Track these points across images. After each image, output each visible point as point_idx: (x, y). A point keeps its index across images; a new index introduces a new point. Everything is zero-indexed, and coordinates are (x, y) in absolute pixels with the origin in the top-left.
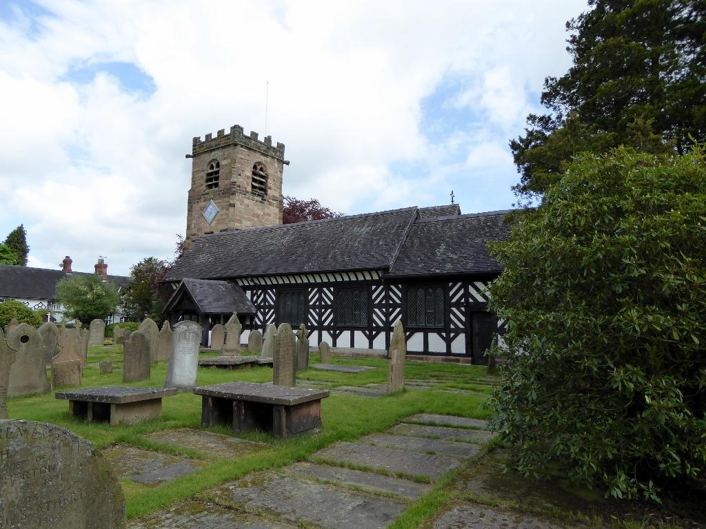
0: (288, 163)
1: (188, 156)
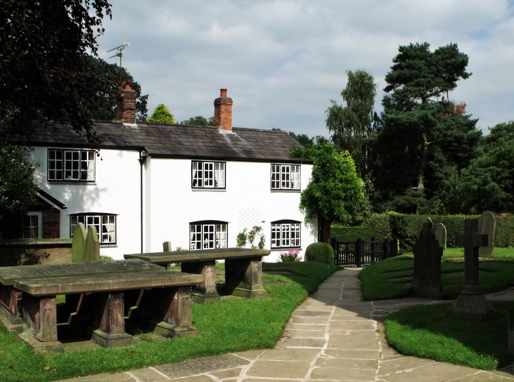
1: (166, 245)
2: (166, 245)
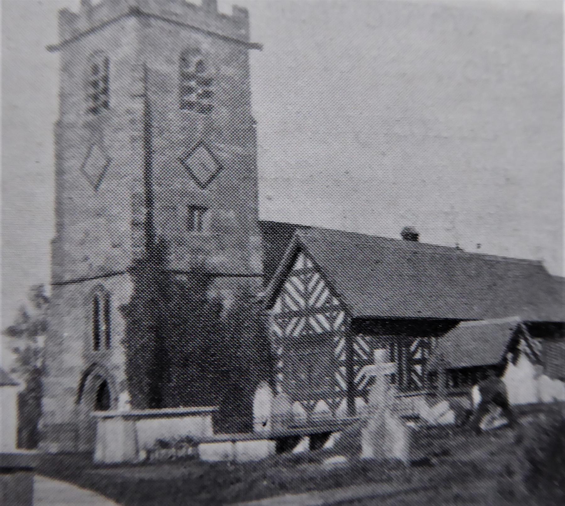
0: (257, 46)
2: (257, 46)
